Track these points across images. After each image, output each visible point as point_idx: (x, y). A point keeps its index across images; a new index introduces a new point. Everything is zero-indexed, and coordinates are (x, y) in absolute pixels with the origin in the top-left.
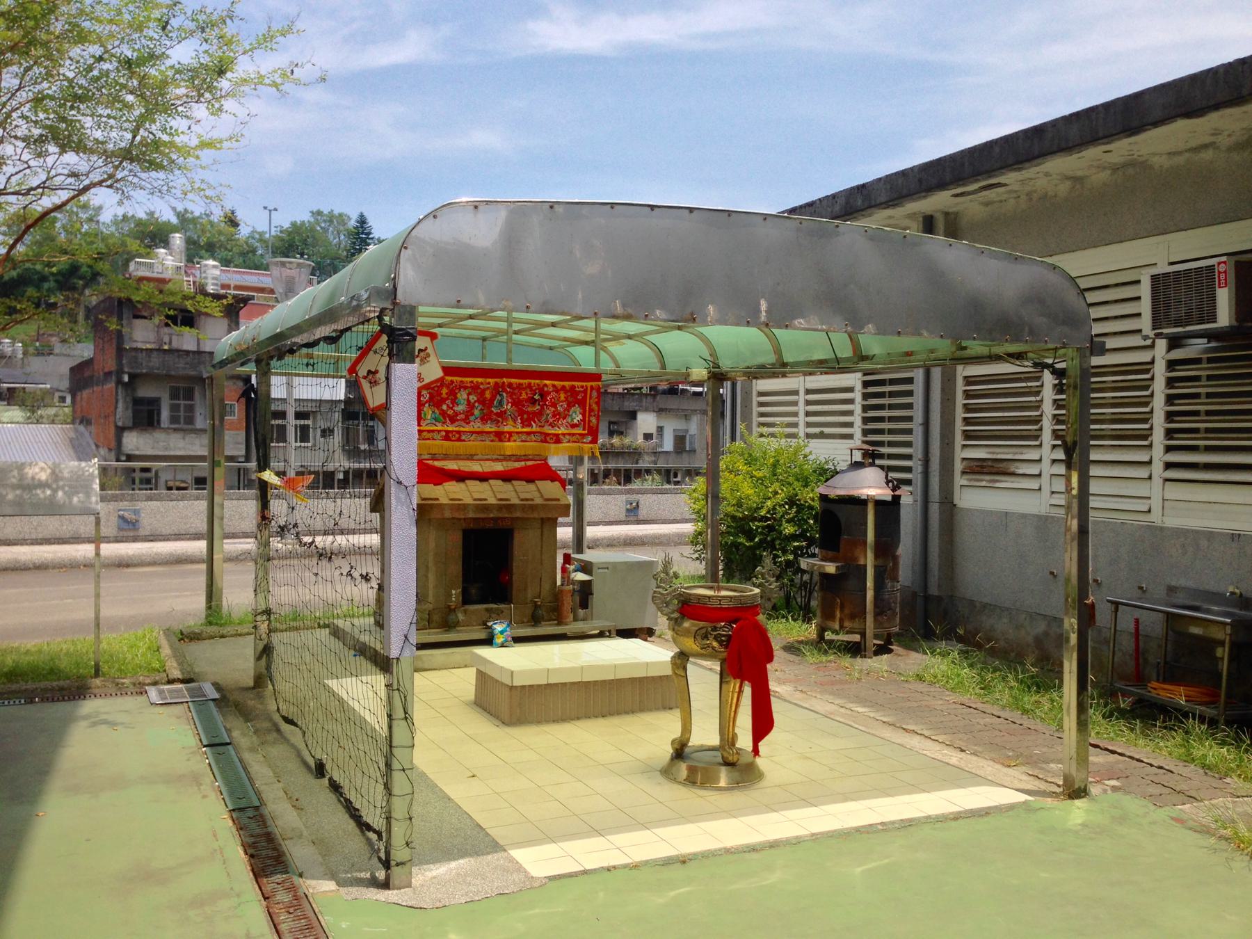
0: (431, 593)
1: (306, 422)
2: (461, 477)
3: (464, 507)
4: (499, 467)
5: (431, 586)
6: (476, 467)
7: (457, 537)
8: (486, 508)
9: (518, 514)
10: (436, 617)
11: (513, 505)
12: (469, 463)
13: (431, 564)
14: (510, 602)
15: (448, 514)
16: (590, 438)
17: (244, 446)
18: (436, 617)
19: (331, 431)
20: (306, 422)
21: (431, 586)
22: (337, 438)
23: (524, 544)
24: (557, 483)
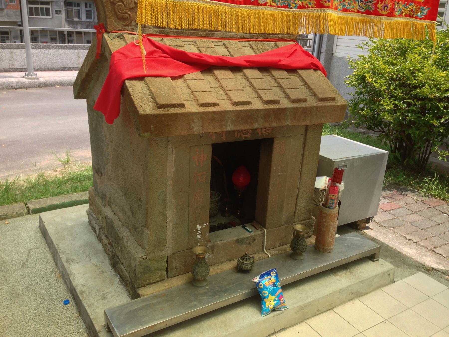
0: (170, 235)
1: (48, 6)
2: (205, 66)
3: (221, 116)
4: (244, 51)
5: (170, 225)
6: (216, 49)
7: (204, 158)
8: (249, 116)
9: (288, 122)
10: (176, 263)
11: (284, 110)
12: (209, 42)
13: (170, 198)
14: (262, 224)
15: (197, 128)
16: (426, 10)
17: (20, 17)
18: (176, 263)
19: (60, 12)
20: (48, 6)
21: (170, 225)
22: (63, 15)
23: (283, 158)
24: (319, 72)
